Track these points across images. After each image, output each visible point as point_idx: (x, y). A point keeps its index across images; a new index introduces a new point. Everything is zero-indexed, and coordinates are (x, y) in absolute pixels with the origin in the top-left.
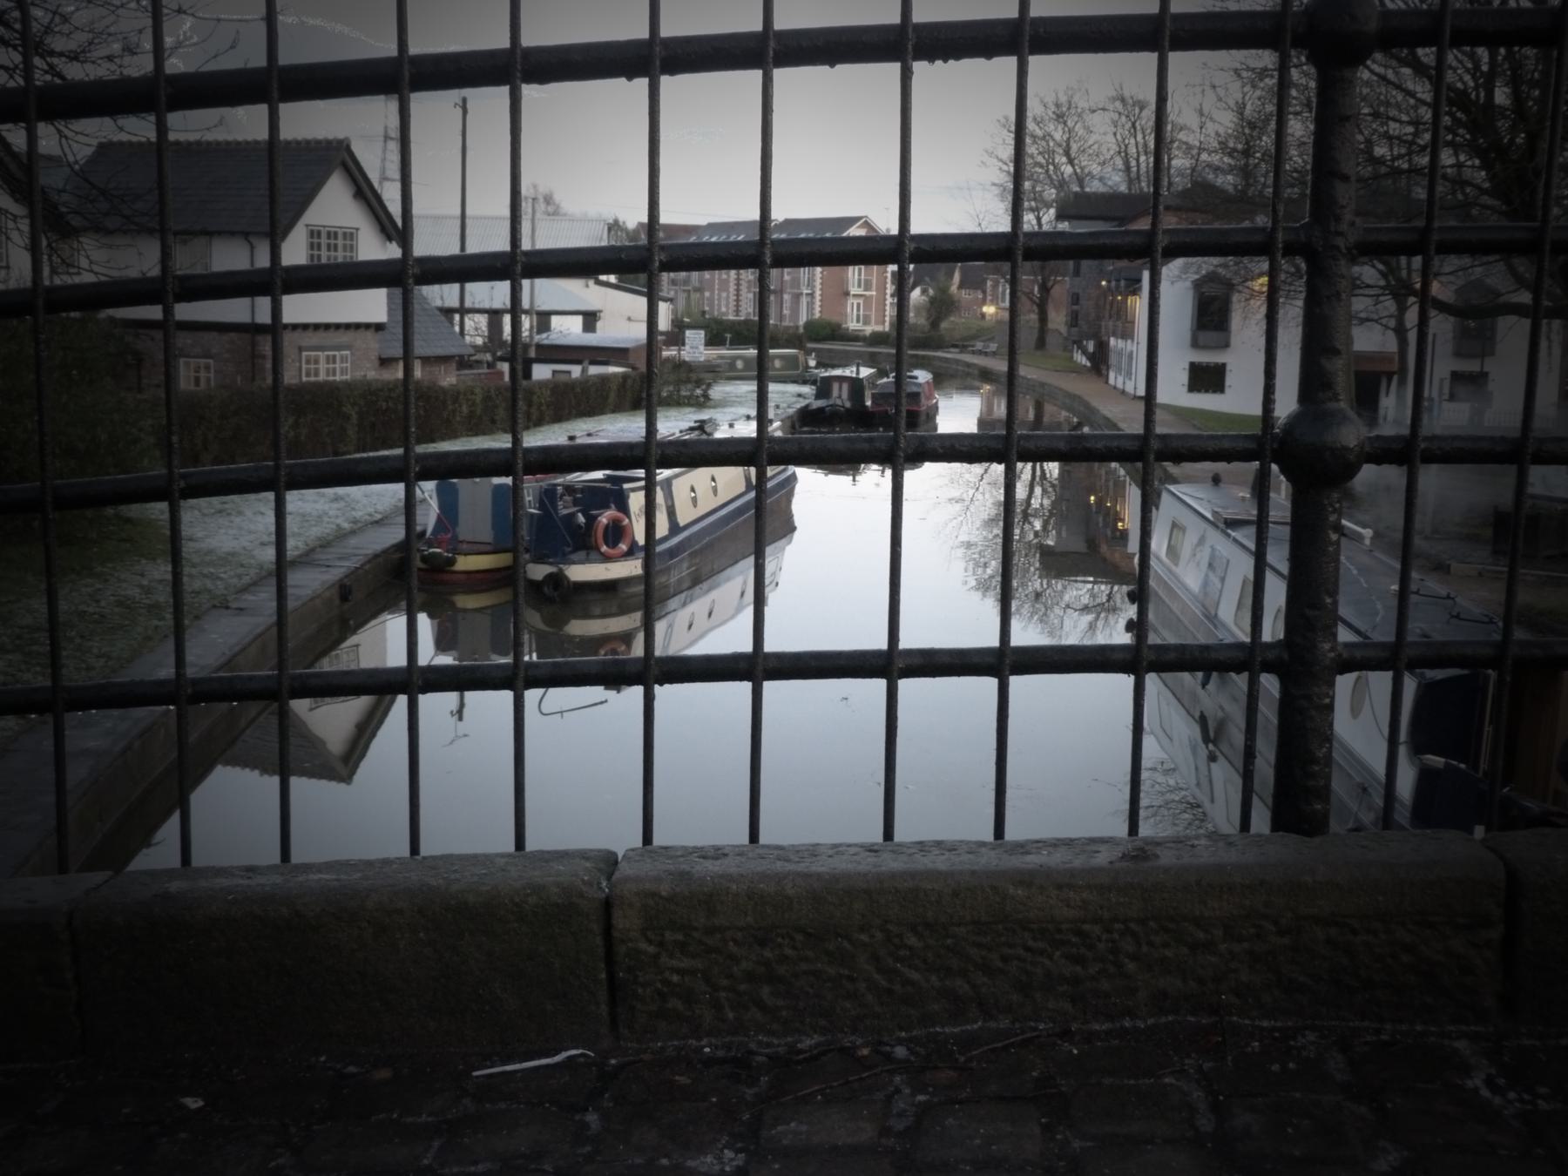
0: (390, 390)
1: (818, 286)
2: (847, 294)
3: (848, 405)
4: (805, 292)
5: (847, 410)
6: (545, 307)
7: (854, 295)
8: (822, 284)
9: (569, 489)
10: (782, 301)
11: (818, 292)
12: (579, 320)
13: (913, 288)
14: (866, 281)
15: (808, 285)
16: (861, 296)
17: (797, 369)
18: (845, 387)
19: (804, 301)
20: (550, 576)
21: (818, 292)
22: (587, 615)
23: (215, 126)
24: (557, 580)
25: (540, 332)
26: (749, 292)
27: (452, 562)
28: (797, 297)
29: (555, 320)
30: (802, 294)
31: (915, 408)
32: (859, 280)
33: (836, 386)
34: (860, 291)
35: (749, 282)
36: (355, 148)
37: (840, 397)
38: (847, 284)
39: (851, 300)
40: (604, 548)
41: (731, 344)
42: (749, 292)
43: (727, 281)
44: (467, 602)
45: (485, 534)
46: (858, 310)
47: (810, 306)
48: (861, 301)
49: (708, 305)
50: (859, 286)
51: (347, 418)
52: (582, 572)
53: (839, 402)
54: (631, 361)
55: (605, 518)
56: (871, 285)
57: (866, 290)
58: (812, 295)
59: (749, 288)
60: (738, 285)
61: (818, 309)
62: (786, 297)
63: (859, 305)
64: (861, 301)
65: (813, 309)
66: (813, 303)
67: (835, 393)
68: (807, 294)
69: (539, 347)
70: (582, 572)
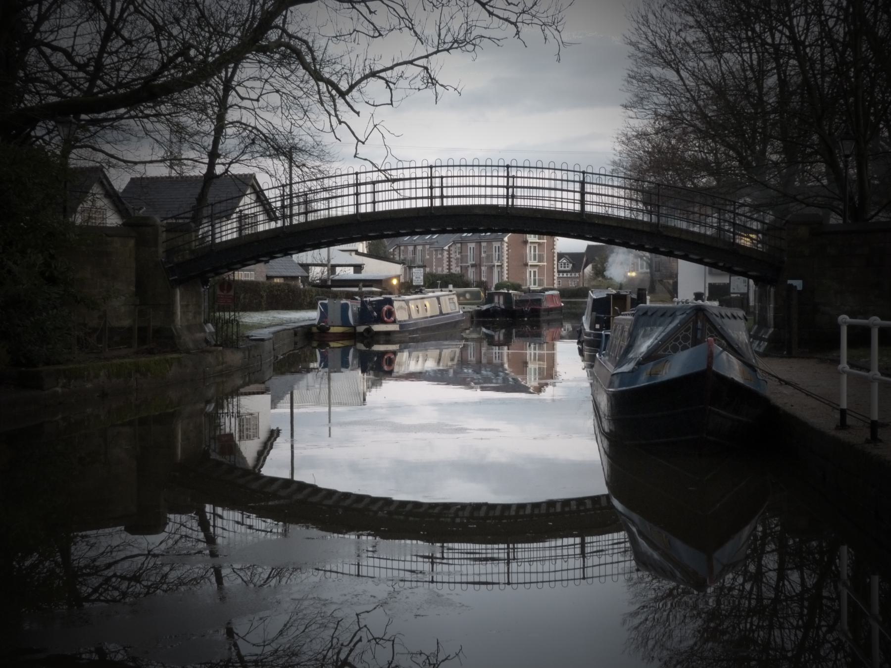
1: (506, 260)
2: (526, 265)
3: (503, 307)
6: (333, 262)
7: (531, 266)
8: (508, 258)
9: (371, 302)
10: (480, 272)
11: (506, 264)
12: (352, 269)
13: (585, 266)
14: (539, 255)
15: (499, 259)
18: (502, 298)
19: (496, 270)
21: (506, 264)
23: (267, 173)
24: (369, 331)
26: (457, 266)
27: (329, 329)
28: (491, 268)
29: (338, 269)
30: (494, 266)
34: (536, 263)
35: (457, 259)
36: (257, 177)
37: (499, 303)
39: (529, 269)
40: (386, 319)
41: (441, 287)
42: (457, 266)
43: (442, 259)
45: (339, 322)
46: (535, 276)
47: (500, 274)
48: (536, 270)
49: (428, 254)
50: (535, 259)
51: (262, 297)
53: (497, 305)
54: (384, 286)
55: (386, 308)
56: (543, 258)
57: (539, 261)
58: (501, 266)
59: (457, 263)
60: (449, 261)
61: (505, 276)
62: (483, 268)
63: (535, 272)
64: (536, 270)
65: (502, 276)
66: (502, 272)
68: (498, 266)
69: (333, 281)
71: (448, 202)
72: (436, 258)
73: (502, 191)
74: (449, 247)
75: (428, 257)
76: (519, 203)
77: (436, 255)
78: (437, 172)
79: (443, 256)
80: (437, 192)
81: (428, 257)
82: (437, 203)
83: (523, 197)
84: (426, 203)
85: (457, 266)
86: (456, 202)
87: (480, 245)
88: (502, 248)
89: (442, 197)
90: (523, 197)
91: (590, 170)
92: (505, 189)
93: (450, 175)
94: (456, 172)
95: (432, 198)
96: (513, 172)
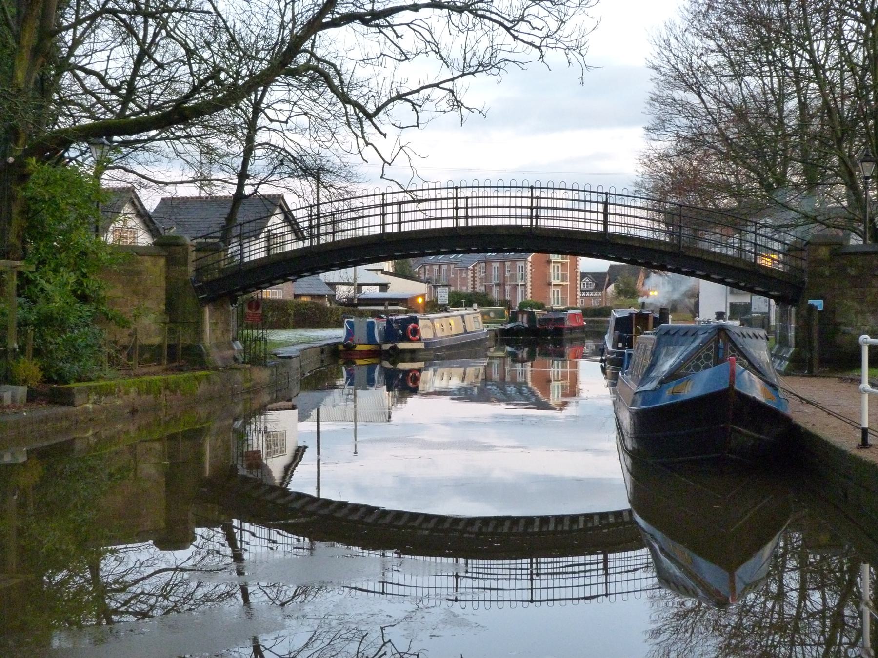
0: (306, 305)
2: (550, 284)
3: (526, 325)
4: (520, 283)
5: (526, 328)
6: (359, 281)
7: (554, 285)
10: (504, 291)
11: (529, 284)
15: (522, 279)
16: (560, 285)
17: (504, 318)
18: (525, 317)
19: (519, 289)
20: (391, 348)
21: (529, 284)
22: (404, 361)
24: (394, 348)
25: (358, 293)
27: (354, 347)
28: (515, 287)
29: (364, 288)
30: (518, 285)
31: (561, 326)
32: (558, 275)
33: (520, 317)
34: (559, 282)
35: (481, 278)
37: (522, 322)
38: (550, 277)
39: (552, 288)
43: (466, 278)
44: (359, 362)
46: (558, 295)
47: (524, 293)
50: (558, 279)
51: (289, 315)
52: (402, 346)
55: (411, 326)
56: (566, 278)
58: (525, 285)
60: (474, 281)
61: (529, 295)
62: (507, 287)
63: (558, 291)
66: (526, 291)
67: (520, 319)
68: (521, 285)
69: (359, 299)
70: (402, 346)
71: (473, 223)
72: (460, 277)
73: (527, 212)
74: (474, 266)
75: (452, 276)
76: (542, 223)
77: (461, 274)
78: (462, 193)
79: (467, 275)
80: (462, 213)
81: (452, 276)
82: (462, 223)
83: (547, 218)
84: (451, 224)
85: (482, 285)
86: (481, 222)
87: (504, 265)
88: (526, 268)
89: (467, 217)
90: (547, 218)
91: (612, 192)
92: (529, 210)
93: (474, 196)
94: (481, 192)
95: (457, 218)
96: (537, 193)
